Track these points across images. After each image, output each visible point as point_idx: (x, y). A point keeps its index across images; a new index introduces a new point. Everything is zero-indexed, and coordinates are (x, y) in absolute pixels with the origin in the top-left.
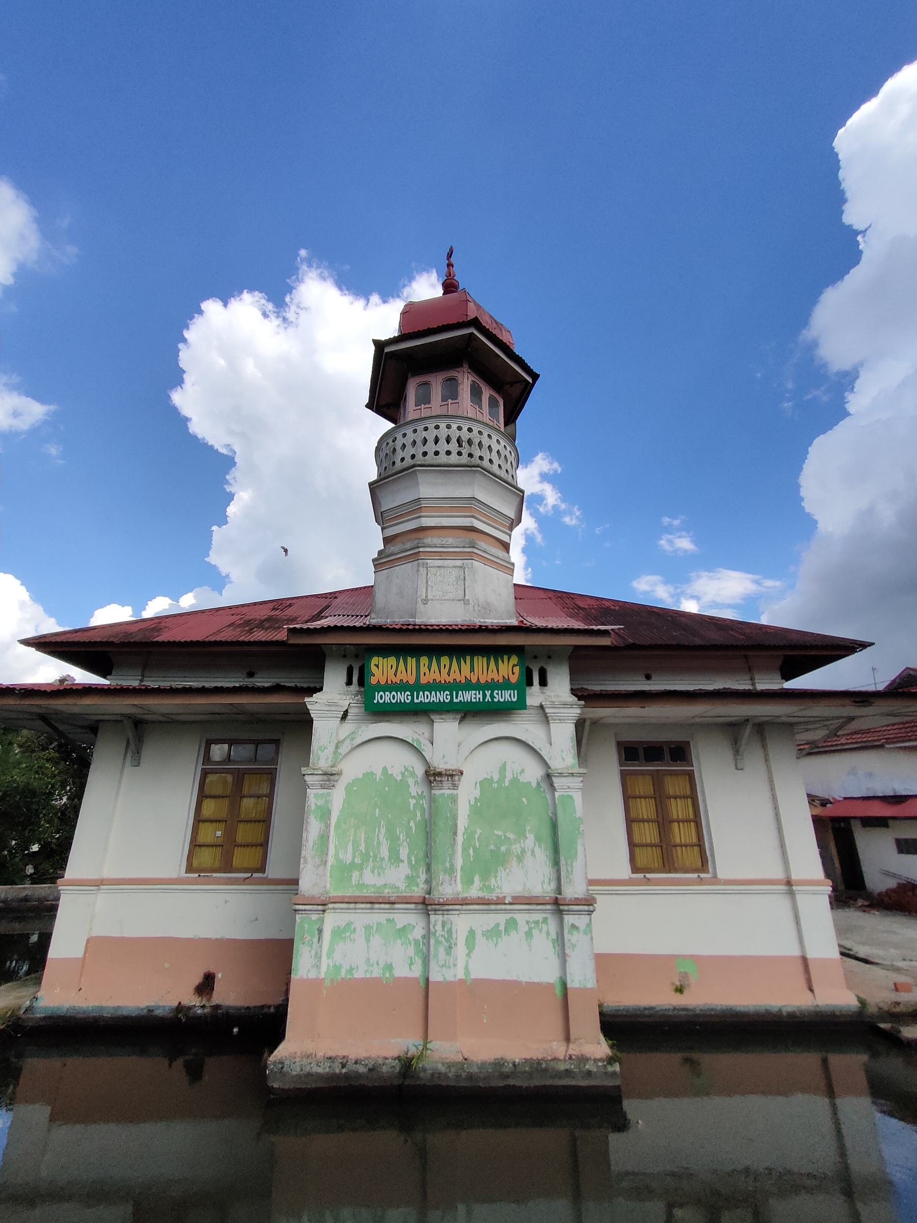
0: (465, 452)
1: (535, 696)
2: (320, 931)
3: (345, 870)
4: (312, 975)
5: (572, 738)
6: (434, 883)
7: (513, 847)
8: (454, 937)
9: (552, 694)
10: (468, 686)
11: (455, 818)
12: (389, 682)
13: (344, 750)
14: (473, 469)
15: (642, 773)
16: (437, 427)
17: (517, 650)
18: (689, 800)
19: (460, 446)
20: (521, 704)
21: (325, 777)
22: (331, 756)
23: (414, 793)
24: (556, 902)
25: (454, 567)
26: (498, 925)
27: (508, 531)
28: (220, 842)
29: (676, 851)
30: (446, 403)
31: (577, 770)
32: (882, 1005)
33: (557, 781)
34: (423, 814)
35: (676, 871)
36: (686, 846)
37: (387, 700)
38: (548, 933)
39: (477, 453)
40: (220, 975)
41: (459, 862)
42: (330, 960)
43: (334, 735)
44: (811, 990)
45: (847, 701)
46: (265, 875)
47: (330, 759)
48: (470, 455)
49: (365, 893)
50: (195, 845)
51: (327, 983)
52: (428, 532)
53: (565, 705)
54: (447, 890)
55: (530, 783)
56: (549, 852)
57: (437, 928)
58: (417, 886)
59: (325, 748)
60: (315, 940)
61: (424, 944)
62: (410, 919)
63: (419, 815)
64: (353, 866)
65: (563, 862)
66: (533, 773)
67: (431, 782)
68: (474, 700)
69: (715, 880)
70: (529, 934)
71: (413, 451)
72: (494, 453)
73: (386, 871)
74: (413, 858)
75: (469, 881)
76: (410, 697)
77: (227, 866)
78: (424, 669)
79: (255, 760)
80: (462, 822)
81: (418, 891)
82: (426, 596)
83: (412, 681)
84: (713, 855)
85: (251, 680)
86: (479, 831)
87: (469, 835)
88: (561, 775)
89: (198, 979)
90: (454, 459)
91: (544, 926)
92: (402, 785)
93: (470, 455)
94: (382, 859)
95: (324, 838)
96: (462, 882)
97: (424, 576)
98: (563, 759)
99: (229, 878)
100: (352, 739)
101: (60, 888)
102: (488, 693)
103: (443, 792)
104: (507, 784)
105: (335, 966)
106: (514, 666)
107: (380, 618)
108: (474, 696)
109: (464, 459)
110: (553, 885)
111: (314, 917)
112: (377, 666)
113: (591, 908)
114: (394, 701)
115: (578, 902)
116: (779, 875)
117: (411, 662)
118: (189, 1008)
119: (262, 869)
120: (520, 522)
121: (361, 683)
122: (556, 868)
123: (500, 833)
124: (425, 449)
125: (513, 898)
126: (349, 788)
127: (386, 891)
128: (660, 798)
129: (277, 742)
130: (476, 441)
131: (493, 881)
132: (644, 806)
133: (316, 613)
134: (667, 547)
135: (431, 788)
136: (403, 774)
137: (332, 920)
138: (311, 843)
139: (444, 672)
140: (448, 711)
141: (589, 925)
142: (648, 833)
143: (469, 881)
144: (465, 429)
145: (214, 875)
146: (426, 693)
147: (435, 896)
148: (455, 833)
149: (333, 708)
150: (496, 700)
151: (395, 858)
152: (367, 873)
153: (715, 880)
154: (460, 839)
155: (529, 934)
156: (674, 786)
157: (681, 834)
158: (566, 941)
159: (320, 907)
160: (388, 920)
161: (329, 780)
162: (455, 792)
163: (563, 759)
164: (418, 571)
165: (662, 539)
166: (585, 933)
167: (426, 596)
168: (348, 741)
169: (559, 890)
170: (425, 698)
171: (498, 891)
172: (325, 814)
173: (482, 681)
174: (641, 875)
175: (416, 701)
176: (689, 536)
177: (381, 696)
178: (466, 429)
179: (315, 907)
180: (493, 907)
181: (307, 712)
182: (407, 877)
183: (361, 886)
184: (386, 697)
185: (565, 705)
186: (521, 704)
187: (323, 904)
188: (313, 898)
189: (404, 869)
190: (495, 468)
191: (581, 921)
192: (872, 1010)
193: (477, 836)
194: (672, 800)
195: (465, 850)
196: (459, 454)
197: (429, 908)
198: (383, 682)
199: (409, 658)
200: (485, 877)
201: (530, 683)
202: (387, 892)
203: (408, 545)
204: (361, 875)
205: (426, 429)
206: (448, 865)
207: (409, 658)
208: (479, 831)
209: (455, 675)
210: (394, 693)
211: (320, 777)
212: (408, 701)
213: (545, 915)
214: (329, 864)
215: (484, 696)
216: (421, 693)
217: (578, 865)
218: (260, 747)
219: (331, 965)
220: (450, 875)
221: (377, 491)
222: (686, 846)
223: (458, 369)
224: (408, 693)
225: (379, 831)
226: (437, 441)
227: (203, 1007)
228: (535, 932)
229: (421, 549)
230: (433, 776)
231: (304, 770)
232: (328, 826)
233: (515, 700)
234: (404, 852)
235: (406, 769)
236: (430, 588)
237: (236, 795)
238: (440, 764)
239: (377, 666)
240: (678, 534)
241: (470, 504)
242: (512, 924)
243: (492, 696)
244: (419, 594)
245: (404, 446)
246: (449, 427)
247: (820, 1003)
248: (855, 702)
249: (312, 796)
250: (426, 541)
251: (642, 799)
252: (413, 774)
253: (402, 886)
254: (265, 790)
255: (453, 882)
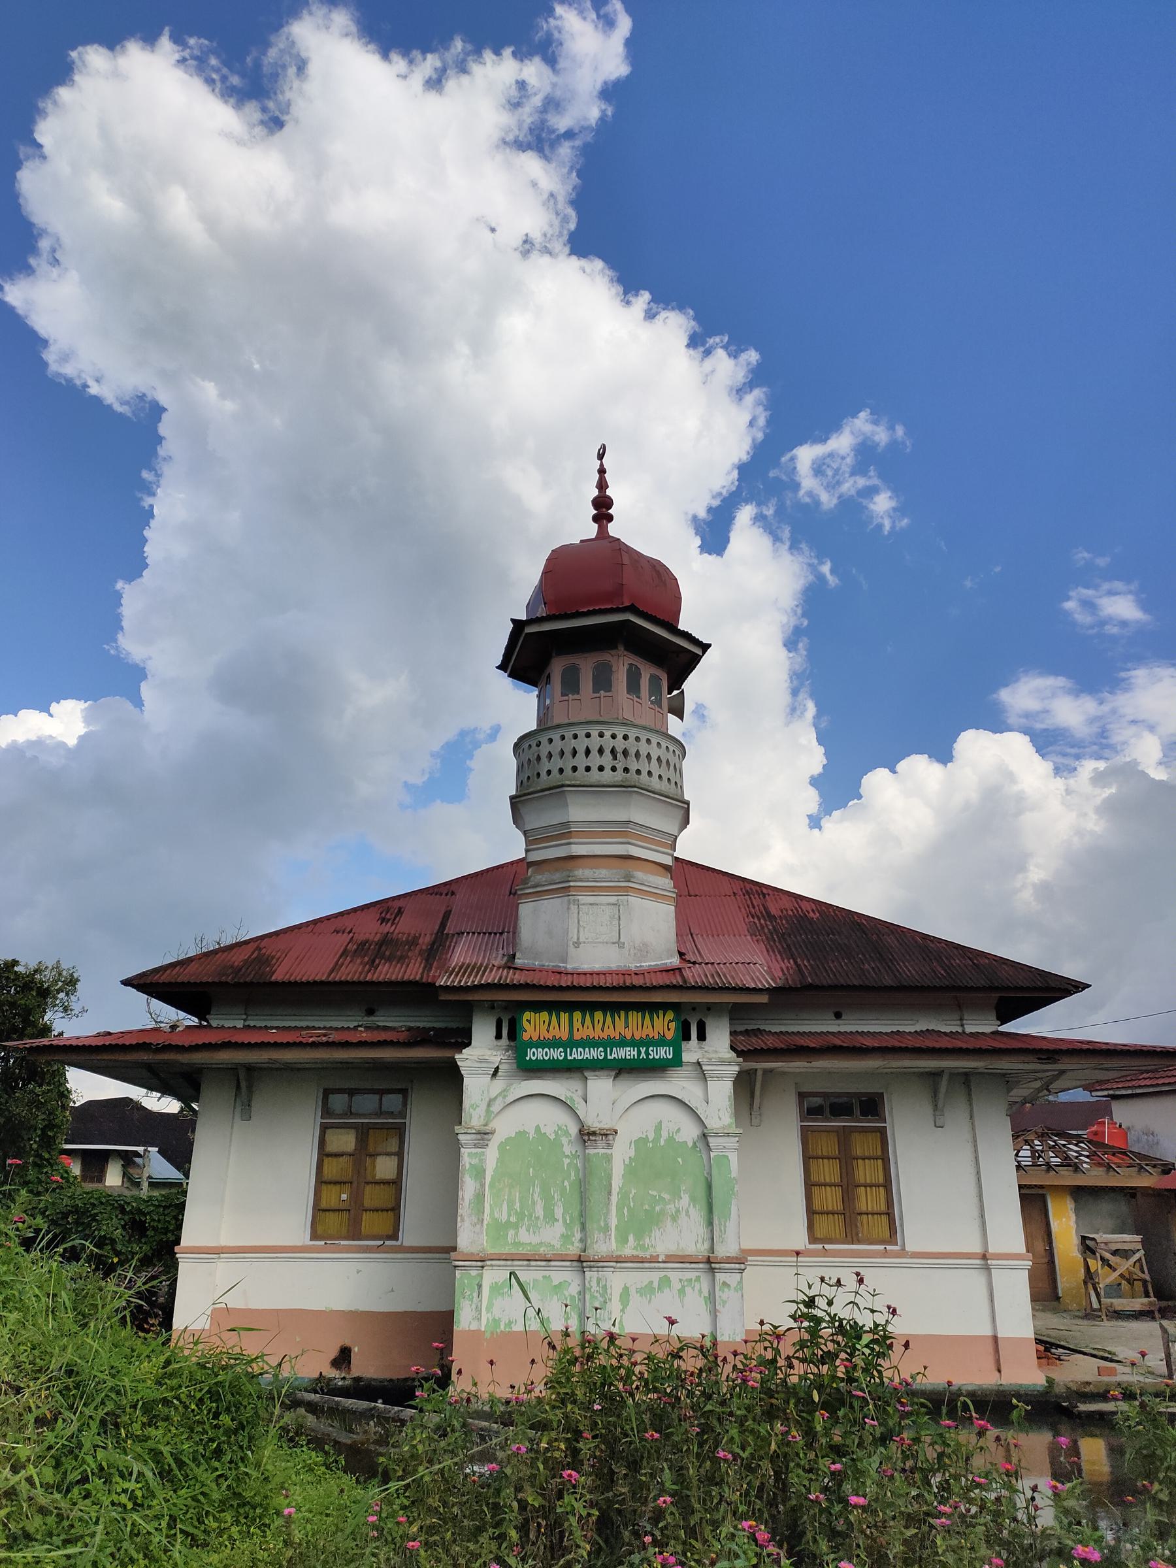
0: (620, 767)
1: (692, 1052)
2: (480, 1286)
3: (500, 1228)
4: (473, 1327)
5: (729, 1097)
6: (589, 1241)
7: (668, 1207)
8: (609, 1291)
9: (711, 1049)
10: (622, 1043)
11: (609, 1177)
12: (542, 1038)
13: (496, 1108)
14: (629, 789)
15: (827, 1131)
16: (588, 735)
17: (675, 1007)
18: (880, 1161)
19: (615, 758)
20: (677, 1062)
21: (479, 1136)
22: (483, 1114)
23: (568, 1153)
24: (709, 1261)
25: (608, 904)
26: (652, 1282)
27: (670, 852)
28: (345, 1206)
29: (862, 1222)
30: (598, 695)
31: (733, 1130)
32: (1071, 1385)
33: (713, 1141)
34: (577, 1174)
35: (859, 1242)
36: (873, 1214)
37: (540, 1057)
38: (700, 1291)
39: (633, 767)
40: (356, 1349)
41: (614, 1221)
42: (490, 1315)
43: (486, 1092)
44: (999, 1371)
45: (1031, 1058)
46: (399, 1243)
47: (482, 1118)
48: (626, 770)
49: (521, 1250)
50: (319, 1210)
51: (488, 1335)
52: (581, 861)
53: (723, 1062)
54: (602, 1247)
55: (686, 1142)
56: (704, 1213)
57: (592, 1284)
58: (573, 1244)
59: (477, 1106)
60: (475, 1294)
61: (579, 1299)
62: (565, 1276)
63: (573, 1174)
64: (508, 1224)
65: (716, 1222)
66: (689, 1132)
67: (585, 1142)
68: (628, 1057)
69: (903, 1253)
70: (682, 1292)
71: (560, 764)
72: (654, 761)
73: (541, 1230)
74: (568, 1218)
75: (623, 1240)
76: (563, 1054)
77: (355, 1233)
78: (577, 1024)
79: (380, 1113)
80: (617, 1182)
81: (574, 1249)
82: (578, 939)
83: (565, 1037)
84: (902, 1225)
85: (370, 1018)
86: (633, 1191)
87: (624, 1195)
88: (716, 1135)
89: (333, 1353)
90: (607, 776)
91: (697, 1285)
92: (555, 1144)
93: (626, 770)
94: (537, 1218)
95: (479, 1197)
96: (617, 1241)
97: (576, 915)
98: (720, 1119)
99: (359, 1246)
100: (505, 1097)
101: (178, 1256)
102: (643, 1050)
103: (597, 1151)
104: (662, 1144)
105: (494, 1320)
106: (670, 1021)
107: (527, 959)
108: (628, 1053)
109: (619, 776)
110: (707, 1245)
111: (474, 1273)
112: (529, 1022)
113: (742, 1266)
114: (546, 1058)
115: (729, 1260)
116: (977, 1249)
117: (565, 1017)
118: (330, 1380)
119: (394, 1236)
120: (688, 823)
121: (512, 1036)
122: (710, 1228)
123: (655, 1193)
124: (575, 762)
125: (667, 1256)
126: (502, 1147)
127: (542, 1249)
128: (846, 1160)
129: (404, 1092)
130: (632, 752)
131: (647, 1240)
132: (826, 1169)
133: (437, 927)
134: (1082, 618)
135: (585, 1148)
136: (556, 1133)
137: (493, 1276)
138: (467, 1202)
139: (598, 1027)
140: (602, 1069)
141: (740, 1282)
142: (831, 1198)
143: (623, 1240)
144: (620, 737)
145: (342, 1242)
146: (580, 1049)
147: (591, 1253)
148: (610, 1193)
149: (484, 1065)
150: (651, 1057)
151: (550, 1217)
152: (522, 1231)
153: (903, 1253)
154: (614, 1198)
155: (682, 1292)
156: (863, 1145)
157: (868, 1200)
158: (717, 1297)
159: (479, 1264)
160: (544, 1277)
161: (483, 1140)
162: (609, 1152)
163: (720, 1119)
164: (568, 908)
165: (1068, 599)
166: (736, 1290)
167: (578, 939)
168: (500, 1099)
169: (712, 1250)
170: (578, 1054)
171: (652, 1250)
172: (480, 1173)
173: (637, 1037)
174: (820, 1246)
175: (569, 1058)
176: (1130, 592)
177: (534, 1053)
178: (621, 736)
179: (474, 1263)
180: (646, 1265)
181: (456, 1068)
182: (562, 1235)
183: (517, 1244)
184: (536, 1054)
185: (723, 1062)
186: (677, 1062)
187: (482, 1261)
188: (472, 1254)
189: (559, 1228)
190: (655, 783)
191: (733, 1279)
192: (1059, 1389)
193: (631, 1196)
194: (860, 1161)
195: (620, 1209)
196: (614, 769)
197: (585, 1264)
198: (535, 1038)
199: (562, 1014)
200: (639, 1236)
201: (687, 1037)
202: (542, 1250)
203: (557, 876)
204: (517, 1234)
205: (575, 736)
206: (602, 1224)
207: (562, 1014)
208: (633, 1191)
209: (609, 1032)
210: (546, 1049)
211: (474, 1136)
212: (561, 1058)
213: (698, 1274)
214: (485, 1222)
215: (639, 1053)
216: (574, 1049)
217: (731, 1226)
218: (841, 1218)
219: (491, 1319)
220: (605, 1233)
221: (519, 805)
222: (873, 1214)
223: (612, 652)
224: (561, 1049)
225: (533, 1190)
226: (588, 752)
227: (344, 1378)
228: (688, 1290)
229: (572, 884)
230: (587, 1135)
231: (457, 1129)
232: (483, 1185)
233: (670, 1057)
234: (559, 1212)
235: (560, 1128)
236: (581, 930)
237: (363, 1153)
238: (594, 1124)
239: (529, 1022)
240: (1106, 586)
241: (624, 830)
242: (665, 1282)
243: (647, 1054)
244: (570, 935)
245: (550, 755)
246: (601, 735)
247: (1004, 1383)
248: (1039, 1059)
249: (466, 1154)
250: (576, 873)
251: (825, 1160)
252: (567, 1133)
253: (557, 1244)
254: (393, 1146)
255: (607, 1240)
